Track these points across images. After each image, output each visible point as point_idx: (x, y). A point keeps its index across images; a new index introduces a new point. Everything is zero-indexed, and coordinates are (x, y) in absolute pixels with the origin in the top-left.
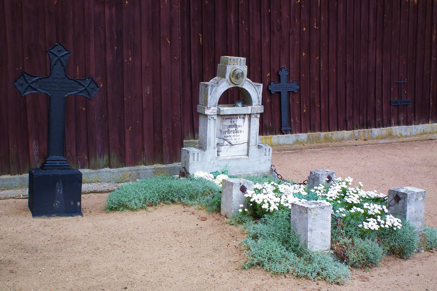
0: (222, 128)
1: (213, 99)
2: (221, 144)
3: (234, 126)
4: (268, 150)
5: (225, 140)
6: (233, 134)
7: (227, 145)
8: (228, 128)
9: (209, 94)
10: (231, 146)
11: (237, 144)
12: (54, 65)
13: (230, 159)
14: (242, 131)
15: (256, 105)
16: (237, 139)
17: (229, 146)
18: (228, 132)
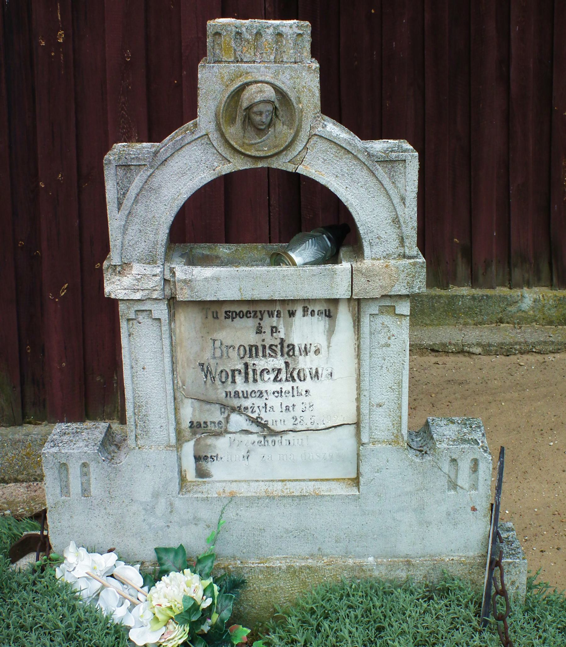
0: (214, 358)
1: (136, 227)
2: (211, 427)
3: (274, 351)
4: (465, 466)
5: (233, 410)
6: (277, 387)
7: (247, 432)
8: (247, 359)
9: (111, 207)
10: (270, 439)
11: (299, 427)
12: (214, 45)
13: (259, 498)
14: (323, 373)
15: (387, 257)
16: (299, 408)
17: (254, 438)
18: (247, 374)
